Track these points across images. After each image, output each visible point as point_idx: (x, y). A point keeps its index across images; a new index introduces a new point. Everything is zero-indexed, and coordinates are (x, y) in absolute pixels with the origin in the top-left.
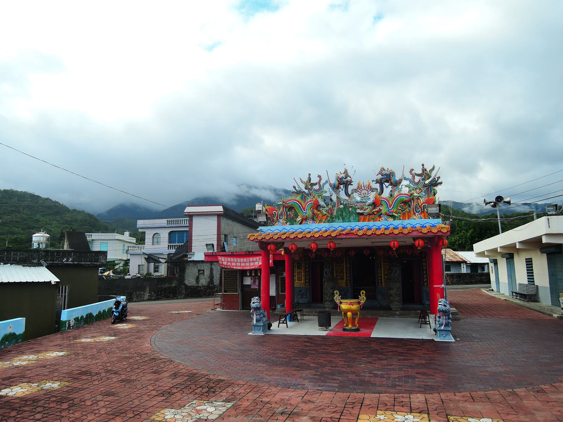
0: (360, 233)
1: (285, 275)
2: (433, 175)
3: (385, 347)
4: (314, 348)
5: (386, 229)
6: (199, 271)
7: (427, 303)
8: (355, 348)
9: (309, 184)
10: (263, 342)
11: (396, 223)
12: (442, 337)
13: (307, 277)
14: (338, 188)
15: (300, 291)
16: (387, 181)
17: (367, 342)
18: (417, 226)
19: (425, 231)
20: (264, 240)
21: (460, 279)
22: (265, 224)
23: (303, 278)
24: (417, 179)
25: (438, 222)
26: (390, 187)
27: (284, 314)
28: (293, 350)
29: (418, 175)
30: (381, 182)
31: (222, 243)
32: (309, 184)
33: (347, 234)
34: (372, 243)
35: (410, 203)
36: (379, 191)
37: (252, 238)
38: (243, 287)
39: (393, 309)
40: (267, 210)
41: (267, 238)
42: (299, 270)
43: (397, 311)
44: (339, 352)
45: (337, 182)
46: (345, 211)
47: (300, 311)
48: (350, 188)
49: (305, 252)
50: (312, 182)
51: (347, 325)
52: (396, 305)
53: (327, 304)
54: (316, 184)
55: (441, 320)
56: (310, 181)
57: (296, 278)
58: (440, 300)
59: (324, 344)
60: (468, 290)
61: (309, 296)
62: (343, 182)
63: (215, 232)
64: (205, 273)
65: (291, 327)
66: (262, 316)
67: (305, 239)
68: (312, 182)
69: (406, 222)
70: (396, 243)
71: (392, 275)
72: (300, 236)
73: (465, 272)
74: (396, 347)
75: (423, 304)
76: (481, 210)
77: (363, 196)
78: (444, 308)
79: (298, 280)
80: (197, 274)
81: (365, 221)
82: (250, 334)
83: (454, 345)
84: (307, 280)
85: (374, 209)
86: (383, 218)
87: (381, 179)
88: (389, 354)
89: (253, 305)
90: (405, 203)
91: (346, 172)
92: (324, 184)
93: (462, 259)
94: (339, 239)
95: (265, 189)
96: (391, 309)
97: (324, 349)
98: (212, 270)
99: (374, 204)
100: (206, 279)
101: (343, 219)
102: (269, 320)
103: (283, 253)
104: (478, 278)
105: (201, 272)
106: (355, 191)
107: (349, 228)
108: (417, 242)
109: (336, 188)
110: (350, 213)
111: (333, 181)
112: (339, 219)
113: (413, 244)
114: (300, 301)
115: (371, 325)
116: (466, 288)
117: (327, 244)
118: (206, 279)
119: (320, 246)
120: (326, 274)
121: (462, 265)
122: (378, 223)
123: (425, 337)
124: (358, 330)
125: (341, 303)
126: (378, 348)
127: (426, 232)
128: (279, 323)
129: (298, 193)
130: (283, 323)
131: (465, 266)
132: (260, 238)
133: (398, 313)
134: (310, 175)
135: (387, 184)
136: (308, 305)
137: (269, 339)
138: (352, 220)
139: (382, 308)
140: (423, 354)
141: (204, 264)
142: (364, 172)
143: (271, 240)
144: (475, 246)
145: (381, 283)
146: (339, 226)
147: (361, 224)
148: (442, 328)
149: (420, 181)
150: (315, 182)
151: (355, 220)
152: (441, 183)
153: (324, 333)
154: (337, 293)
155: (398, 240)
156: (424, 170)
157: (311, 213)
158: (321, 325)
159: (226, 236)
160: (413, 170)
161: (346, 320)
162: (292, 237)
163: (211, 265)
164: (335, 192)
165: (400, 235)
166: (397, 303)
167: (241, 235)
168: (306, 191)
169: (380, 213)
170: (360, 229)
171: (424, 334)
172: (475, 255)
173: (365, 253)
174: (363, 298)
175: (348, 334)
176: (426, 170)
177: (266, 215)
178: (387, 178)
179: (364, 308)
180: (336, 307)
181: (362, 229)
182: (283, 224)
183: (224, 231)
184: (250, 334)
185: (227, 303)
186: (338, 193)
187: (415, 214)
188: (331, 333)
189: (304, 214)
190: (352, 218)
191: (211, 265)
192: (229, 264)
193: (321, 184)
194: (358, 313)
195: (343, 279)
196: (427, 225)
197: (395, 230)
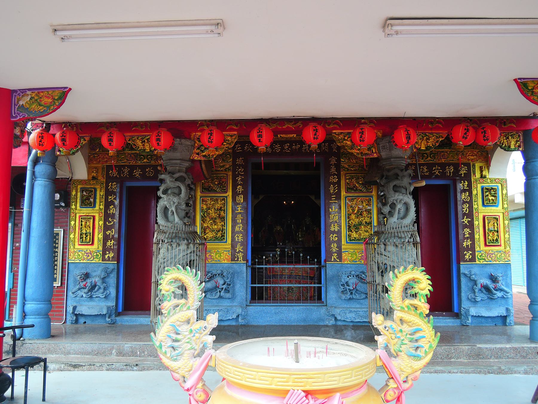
7: (473, 311)
23: (99, 236)
42: (86, 211)
61: (112, 291)
195: (222, 238)
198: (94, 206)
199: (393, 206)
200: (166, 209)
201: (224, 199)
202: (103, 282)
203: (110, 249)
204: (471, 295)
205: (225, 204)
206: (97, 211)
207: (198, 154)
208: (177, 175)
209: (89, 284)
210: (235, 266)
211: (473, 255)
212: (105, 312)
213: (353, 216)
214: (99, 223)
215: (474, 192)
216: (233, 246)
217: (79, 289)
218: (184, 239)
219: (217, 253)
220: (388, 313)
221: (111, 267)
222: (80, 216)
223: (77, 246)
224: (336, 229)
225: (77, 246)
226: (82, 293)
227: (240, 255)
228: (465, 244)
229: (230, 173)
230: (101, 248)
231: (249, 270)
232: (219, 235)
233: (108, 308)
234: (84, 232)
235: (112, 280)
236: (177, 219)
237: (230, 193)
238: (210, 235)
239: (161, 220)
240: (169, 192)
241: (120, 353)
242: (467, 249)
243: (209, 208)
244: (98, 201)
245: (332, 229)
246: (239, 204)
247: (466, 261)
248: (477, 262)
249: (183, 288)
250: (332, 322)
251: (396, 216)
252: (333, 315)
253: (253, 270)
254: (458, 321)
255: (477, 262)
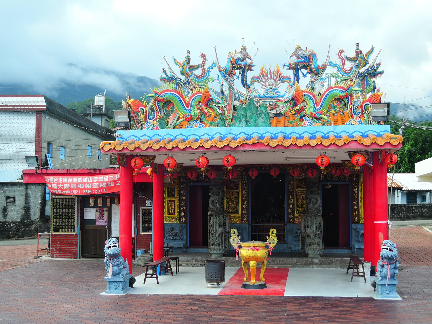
0: (274, 143)
1: (149, 205)
2: (371, 60)
3: (307, 310)
4: (205, 313)
5: (310, 138)
6: (7, 198)
7: (357, 246)
8: (265, 312)
9: (188, 67)
10: (125, 306)
11: (326, 129)
12: (385, 294)
13: (183, 209)
14: (231, 74)
15: (172, 230)
16: (305, 67)
17: (280, 303)
18: (355, 134)
19: (367, 142)
20: (125, 151)
21: (398, 213)
22: (127, 127)
23: (177, 210)
24: (348, 65)
25: (385, 128)
26: (309, 75)
27: (152, 263)
28: (174, 317)
29: (350, 59)
30: (295, 68)
31: (43, 156)
32: (188, 67)
33: (253, 145)
34: (287, 158)
35: (346, 100)
36: (292, 80)
37: (107, 148)
38: (84, 223)
39: (310, 256)
40: (129, 105)
41: (131, 148)
42: (171, 198)
43: (316, 258)
44: (243, 318)
45: (230, 67)
46: (250, 109)
47: (175, 259)
48: (250, 75)
49: (183, 171)
50: (191, 63)
51: (249, 279)
52: (315, 249)
53: (214, 249)
54: (198, 67)
55: (384, 270)
56: (188, 63)
57: (166, 210)
58: (385, 242)
59: (218, 308)
60: (405, 227)
61: (185, 236)
62: (239, 66)
63: (33, 138)
64: (17, 202)
65: (164, 284)
66: (122, 267)
67: (190, 150)
68: (191, 63)
69: (339, 128)
70: (325, 159)
71: (310, 206)
72: (182, 146)
73: (399, 203)
74: (323, 309)
75: (351, 248)
76: (421, 116)
77: (269, 87)
78: (389, 253)
79: (170, 213)
80: (4, 204)
81: (279, 126)
82: (104, 293)
83: (402, 304)
84: (183, 214)
85: (292, 108)
86: (307, 122)
87: (296, 64)
88: (315, 319)
89: (107, 251)
90: (339, 99)
91: (244, 50)
92: (211, 67)
93: (396, 184)
94: (241, 151)
95: (108, 72)
96: (306, 256)
97: (220, 315)
98: (27, 197)
99: (295, 101)
100: (18, 211)
101: (247, 121)
102: (131, 273)
103: (149, 171)
104: (418, 211)
105: (10, 200)
106: (257, 79)
107: (255, 136)
108: (355, 159)
109: (228, 74)
110: (258, 114)
111: (225, 63)
112: (240, 121)
113: (349, 162)
114: (171, 245)
115: (280, 277)
116: (402, 226)
117: (318, 158)
118: (18, 211)
119: (211, 163)
120: (213, 204)
121: (396, 192)
122: (299, 130)
123: (361, 295)
124: (263, 286)
125: (240, 247)
126: (298, 312)
127: (368, 143)
128: (146, 277)
129: (169, 80)
130: (151, 277)
131: (400, 194)
132: (119, 148)
133: (317, 261)
134: (188, 52)
135: (305, 71)
136: (185, 250)
137: (129, 303)
138: (260, 124)
139: (292, 254)
140: (364, 318)
141: (15, 188)
142: (271, 53)
143: (138, 151)
144: (418, 165)
145: (293, 218)
146: (240, 132)
147: (274, 130)
148: (387, 282)
149: (352, 68)
150: (196, 64)
151: (264, 124)
152: (381, 73)
153: (215, 291)
154: (234, 233)
155: (328, 155)
156: (359, 52)
157: (198, 111)
158: (210, 279)
159: (49, 144)
160: (342, 51)
161: (246, 272)
162: (169, 147)
163: (27, 189)
164: (227, 80)
165: (332, 147)
166: (315, 247)
167: (72, 143)
168: (183, 78)
169: (302, 114)
170: (271, 138)
171: (360, 288)
172: (417, 179)
173: (272, 173)
174: (272, 240)
175: (250, 293)
176: (361, 53)
177: (129, 113)
178: (304, 63)
179: (275, 254)
180: (231, 253)
181: (276, 138)
182: (154, 127)
183: (46, 136)
184: (104, 293)
185: (59, 247)
186: (231, 83)
187: (352, 116)
188: (225, 291)
189: (187, 113)
190: (260, 121)
191: (27, 189)
192: (60, 186)
193: (206, 67)
194: (266, 262)
195: (237, 212)
196: (370, 134)
197: (311, 141)
198: (175, 196)
199: (310, 200)
200: (213, 201)
201: (238, 192)
202: (181, 232)
203: (183, 217)
204: (356, 239)
205: (238, 195)
206: (176, 199)
207: (226, 176)
208: (218, 187)
209: (174, 233)
210: (243, 224)
211: (359, 219)
212: (182, 246)
213: (300, 201)
214: (177, 204)
215: (360, 188)
216: (242, 214)
217: (169, 236)
218: (221, 214)
219: (235, 218)
220: (269, 237)
221: (184, 225)
222: (168, 201)
223: (167, 215)
224: (292, 206)
225: (167, 215)
226: (171, 237)
227: (245, 219)
228: (354, 214)
229: (240, 180)
230: (178, 216)
231: (250, 226)
232: (235, 210)
233: (184, 244)
234: (170, 208)
235: (184, 232)
236: (218, 206)
237: (240, 189)
238: (231, 210)
239: (211, 206)
240: (214, 194)
241: (197, 261)
242: (356, 216)
243: (230, 197)
244: (176, 193)
245: (290, 207)
246: (244, 195)
247: (355, 222)
248: (360, 223)
249: (235, 232)
250: (289, 251)
251: (311, 204)
252: (290, 248)
253: (252, 227)
254: (350, 251)
255: (360, 223)
